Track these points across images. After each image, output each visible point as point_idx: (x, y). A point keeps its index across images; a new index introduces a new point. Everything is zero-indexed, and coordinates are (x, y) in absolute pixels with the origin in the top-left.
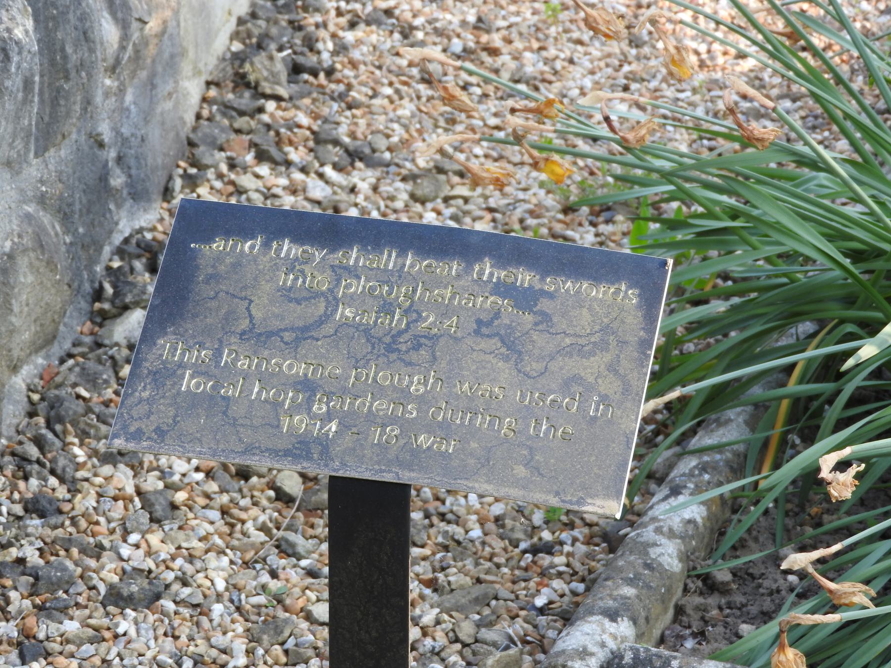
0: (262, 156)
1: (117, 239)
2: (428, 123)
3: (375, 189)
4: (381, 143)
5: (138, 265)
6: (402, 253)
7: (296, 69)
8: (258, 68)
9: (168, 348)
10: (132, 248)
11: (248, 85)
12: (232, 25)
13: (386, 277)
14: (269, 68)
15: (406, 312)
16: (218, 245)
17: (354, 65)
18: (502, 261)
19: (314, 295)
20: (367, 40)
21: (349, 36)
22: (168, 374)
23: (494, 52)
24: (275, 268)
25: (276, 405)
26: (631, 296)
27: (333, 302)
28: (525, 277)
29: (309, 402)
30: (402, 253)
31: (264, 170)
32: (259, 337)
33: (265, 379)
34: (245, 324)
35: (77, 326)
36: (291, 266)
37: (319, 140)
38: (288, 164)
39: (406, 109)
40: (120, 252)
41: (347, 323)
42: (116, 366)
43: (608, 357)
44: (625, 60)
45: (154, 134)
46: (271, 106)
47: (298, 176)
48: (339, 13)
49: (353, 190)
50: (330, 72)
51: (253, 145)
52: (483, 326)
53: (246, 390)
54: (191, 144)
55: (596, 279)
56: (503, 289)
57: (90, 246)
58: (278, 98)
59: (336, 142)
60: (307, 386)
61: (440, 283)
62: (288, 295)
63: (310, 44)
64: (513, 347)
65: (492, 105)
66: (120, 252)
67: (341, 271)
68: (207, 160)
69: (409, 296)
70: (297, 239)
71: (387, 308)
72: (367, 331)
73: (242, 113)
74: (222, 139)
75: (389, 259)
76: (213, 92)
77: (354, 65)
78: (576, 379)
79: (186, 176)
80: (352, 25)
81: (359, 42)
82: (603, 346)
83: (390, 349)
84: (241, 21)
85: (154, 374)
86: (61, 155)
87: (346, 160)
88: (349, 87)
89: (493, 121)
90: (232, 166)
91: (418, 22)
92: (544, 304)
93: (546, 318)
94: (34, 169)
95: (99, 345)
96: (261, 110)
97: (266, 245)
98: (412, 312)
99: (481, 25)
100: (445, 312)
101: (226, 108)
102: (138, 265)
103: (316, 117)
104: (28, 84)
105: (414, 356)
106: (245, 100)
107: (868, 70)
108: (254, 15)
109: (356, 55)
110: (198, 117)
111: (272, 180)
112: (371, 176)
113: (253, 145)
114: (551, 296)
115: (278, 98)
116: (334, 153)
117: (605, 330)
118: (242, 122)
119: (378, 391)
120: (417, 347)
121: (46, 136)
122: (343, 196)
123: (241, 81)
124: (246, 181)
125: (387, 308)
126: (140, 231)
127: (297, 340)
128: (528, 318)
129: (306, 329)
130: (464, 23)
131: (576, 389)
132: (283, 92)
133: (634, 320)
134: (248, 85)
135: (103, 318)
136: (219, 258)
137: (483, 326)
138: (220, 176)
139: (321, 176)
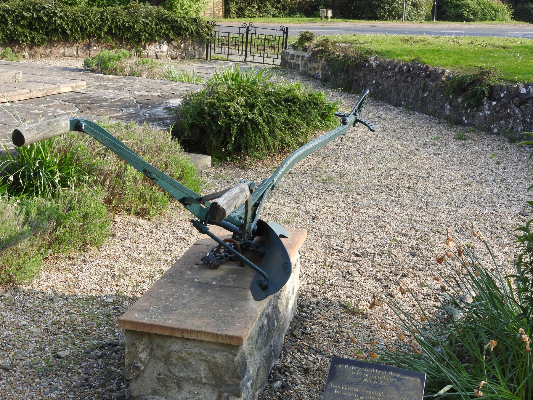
0: (298, 351)
1: (272, 366)
2: (331, 346)
3: (322, 359)
4: (322, 350)
5: (277, 372)
6: (375, 370)
7: (303, 333)
8: (296, 332)
9: (332, 385)
10: (275, 368)
11: (294, 336)
12: (289, 324)
13: (372, 374)
14: (298, 332)
15: (377, 381)
16: (340, 366)
17: (314, 333)
18: (394, 372)
19: (359, 376)
20: (316, 328)
21: (313, 327)
22: (332, 390)
23: (343, 332)
24: (351, 371)
25: (353, 397)
26: (419, 380)
27: (363, 378)
28: (399, 375)
29: (359, 397)
30: (375, 370)
31: (299, 354)
32: (349, 384)
33: (351, 392)
34: (346, 381)
35: (267, 384)
36: (354, 371)
37: (310, 348)
38: (304, 353)
39: (326, 343)
40: (273, 369)
41: (365, 382)
42: (275, 392)
43: (415, 391)
44: (370, 336)
45: (279, 344)
46: (299, 340)
47: (306, 355)
48: (310, 322)
49: (317, 359)
50: (310, 334)
51: (296, 348)
52: (392, 384)
53: (347, 394)
54: (284, 347)
55: (412, 376)
56: (395, 377)
57: (269, 366)
58: (300, 339)
59: (313, 349)
60: (359, 394)
61: (383, 375)
62: (354, 376)
63: (305, 328)
64: (397, 388)
65: (344, 343)
66: (273, 369)
67: (364, 372)
68: (288, 351)
69: (377, 378)
70: (355, 365)
71: (373, 380)
72: (369, 384)
73: (293, 342)
74: (290, 347)
75: (373, 371)
76: (287, 337)
77: (314, 333)
78: (410, 395)
79: (283, 354)
80: (313, 325)
81: (315, 328)
82: (414, 389)
83: (374, 387)
84: (291, 323)
85: (329, 389)
86: (268, 347)
87: (315, 353)
88: (314, 338)
89: (344, 347)
90: (293, 353)
91: (327, 325)
92: (403, 381)
93: (403, 383)
94: (263, 351)
95: (271, 388)
96: (297, 341)
97: (349, 366)
98: (378, 381)
99: (339, 326)
100: (384, 381)
101: (290, 340)
102: (277, 372)
103: (308, 343)
104: (265, 333)
105: (379, 389)
106: (293, 339)
107: (142, 335)
108: (293, 321)
109: (315, 331)
110: (284, 342)
111: (301, 356)
112: (321, 356)
113: (296, 348)
114: (404, 379)
115: (300, 339)
116: (313, 351)
117: (414, 386)
118: (293, 344)
119: (372, 395)
120: (379, 387)
121: (266, 344)
122: (315, 360)
123: (292, 335)
124: (296, 356)
125: (373, 380)
126: (276, 365)
127: (356, 385)
128: (400, 383)
129: (358, 383)
130: (336, 326)
131: (410, 397)
132: (301, 338)
133: (419, 384)
134: (294, 336)
135: (271, 382)
136: (340, 368)
137: (392, 384)
138: (291, 354)
139: (311, 356)
